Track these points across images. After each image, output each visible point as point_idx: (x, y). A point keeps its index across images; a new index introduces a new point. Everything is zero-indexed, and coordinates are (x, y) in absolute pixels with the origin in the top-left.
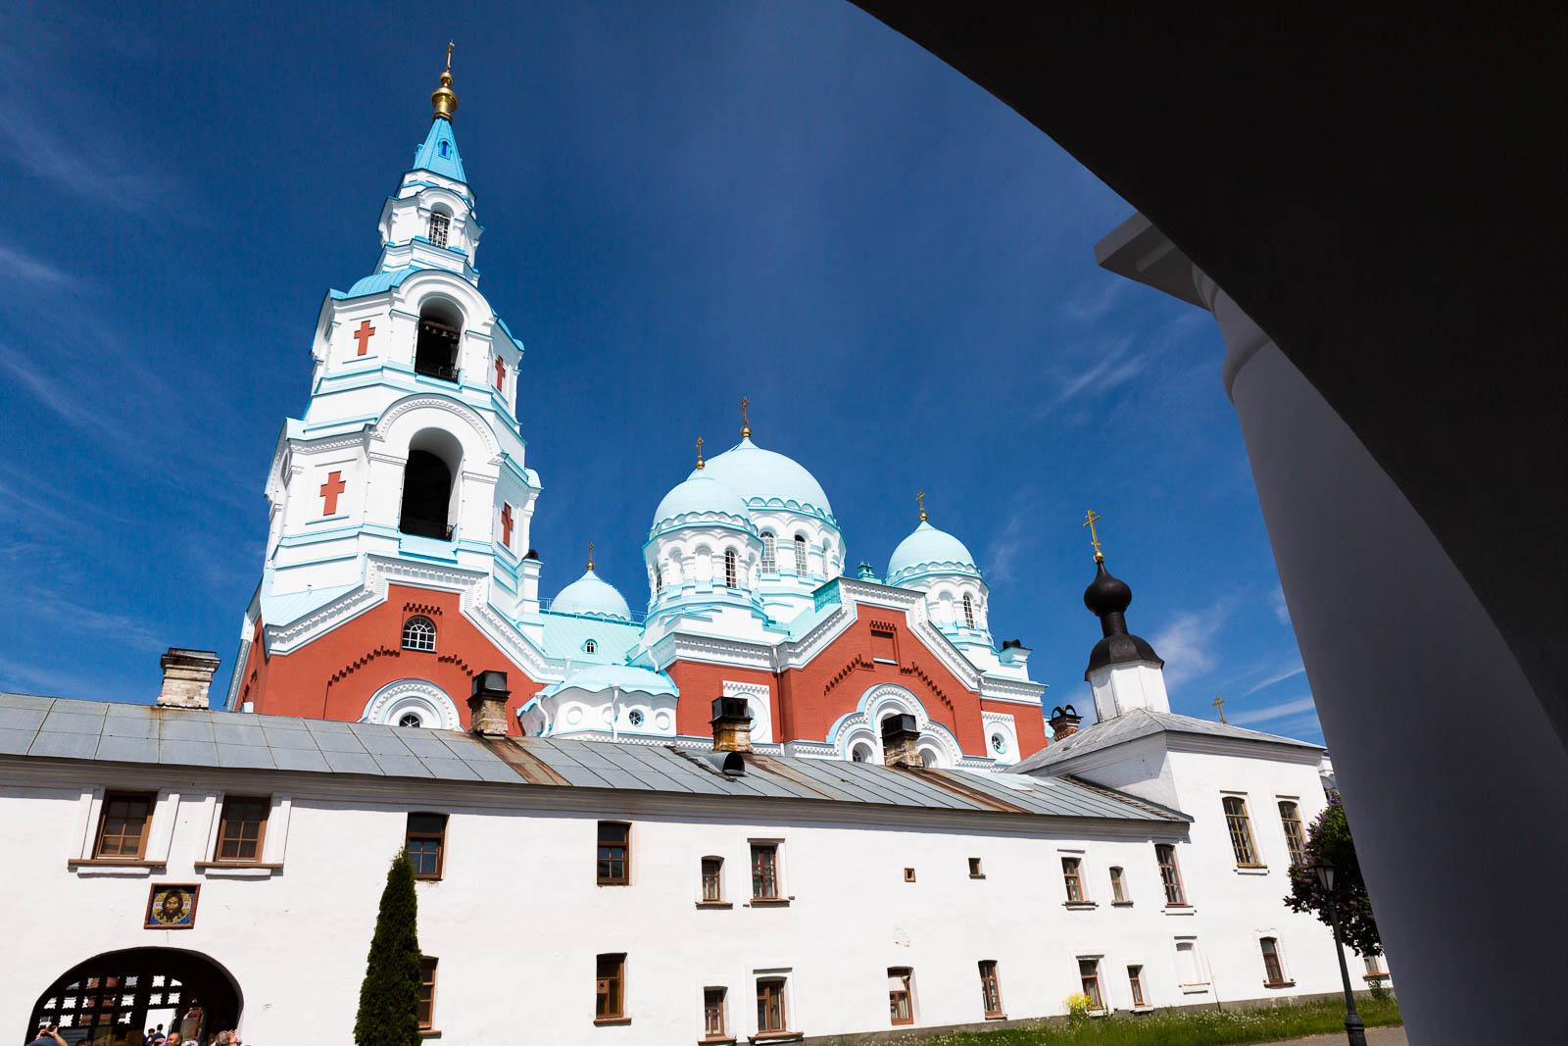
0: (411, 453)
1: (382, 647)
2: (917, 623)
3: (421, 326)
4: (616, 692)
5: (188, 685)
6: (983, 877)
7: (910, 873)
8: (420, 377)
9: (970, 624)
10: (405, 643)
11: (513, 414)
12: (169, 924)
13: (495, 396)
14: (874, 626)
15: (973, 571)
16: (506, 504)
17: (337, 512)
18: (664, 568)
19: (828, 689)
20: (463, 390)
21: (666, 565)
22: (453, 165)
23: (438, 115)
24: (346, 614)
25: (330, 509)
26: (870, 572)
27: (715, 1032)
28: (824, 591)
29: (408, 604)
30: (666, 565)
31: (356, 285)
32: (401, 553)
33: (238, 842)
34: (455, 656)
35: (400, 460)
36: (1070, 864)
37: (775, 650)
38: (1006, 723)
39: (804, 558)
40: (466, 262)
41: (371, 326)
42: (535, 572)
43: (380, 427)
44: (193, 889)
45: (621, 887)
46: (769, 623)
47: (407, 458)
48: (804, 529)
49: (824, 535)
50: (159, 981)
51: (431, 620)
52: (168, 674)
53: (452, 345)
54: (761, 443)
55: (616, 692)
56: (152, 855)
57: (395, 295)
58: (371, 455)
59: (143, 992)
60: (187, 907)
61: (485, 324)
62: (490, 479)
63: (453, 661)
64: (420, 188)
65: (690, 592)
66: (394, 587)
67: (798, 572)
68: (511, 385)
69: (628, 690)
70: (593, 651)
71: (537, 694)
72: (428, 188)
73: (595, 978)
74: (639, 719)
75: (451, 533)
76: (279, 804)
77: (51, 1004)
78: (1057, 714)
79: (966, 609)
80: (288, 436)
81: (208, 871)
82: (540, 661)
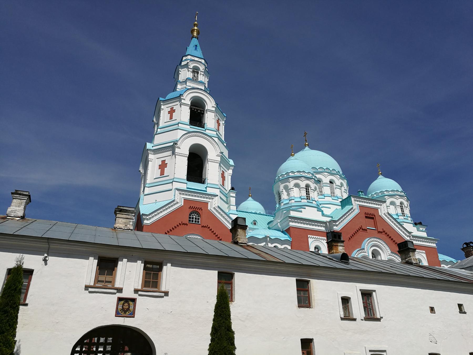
3: (191, 109)
4: (268, 238)
5: (124, 221)
6: (465, 313)
7: (432, 309)
9: (403, 214)
10: (190, 221)
11: (223, 140)
12: (125, 315)
13: (217, 132)
14: (366, 214)
15: (403, 194)
17: (165, 174)
19: (350, 239)
20: (207, 130)
22: (199, 53)
23: (193, 37)
24: (169, 210)
25: (162, 173)
26: (363, 194)
28: (344, 203)
29: (190, 207)
31: (169, 95)
32: (187, 188)
33: (151, 281)
34: (207, 225)
35: (186, 155)
38: (422, 254)
39: (333, 190)
40: (205, 86)
42: (234, 195)
43: (179, 143)
44: (134, 300)
45: (306, 309)
48: (334, 179)
49: (341, 181)
51: (197, 211)
52: (118, 215)
53: (201, 115)
54: (312, 148)
55: (268, 238)
56: (117, 285)
57: (182, 97)
60: (131, 308)
61: (213, 107)
62: (217, 162)
63: (206, 227)
65: (293, 201)
66: (185, 200)
67: (332, 195)
68: (222, 129)
69: (272, 238)
70: (256, 224)
72: (191, 61)
73: (301, 349)
75: (205, 179)
76: (166, 265)
77: (78, 349)
78: (465, 246)
79: (401, 208)
80: (147, 148)
81: (140, 293)
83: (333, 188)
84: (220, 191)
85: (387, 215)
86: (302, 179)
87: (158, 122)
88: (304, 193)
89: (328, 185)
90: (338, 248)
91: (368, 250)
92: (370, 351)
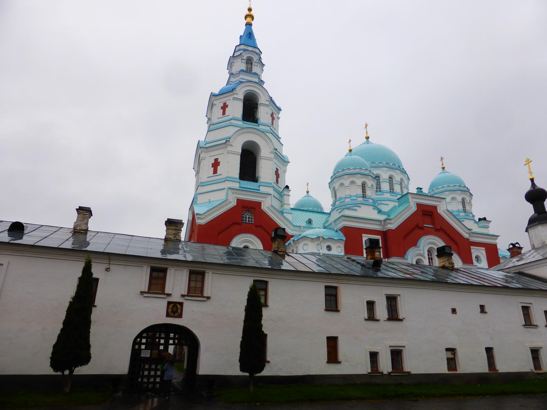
0: (242, 150)
1: (235, 222)
2: (442, 210)
4: (321, 239)
5: (174, 232)
7: (454, 311)
8: (245, 122)
13: (271, 127)
16: (276, 168)
18: (338, 191)
21: (338, 189)
27: (374, 369)
29: (243, 206)
30: (338, 189)
34: (261, 225)
36: (526, 310)
37: (383, 222)
39: (393, 186)
41: (227, 104)
43: (231, 140)
44: (181, 304)
46: (380, 212)
47: (241, 152)
50: (172, 335)
53: (255, 109)
55: (321, 239)
58: (228, 152)
59: (167, 339)
61: (267, 100)
64: (241, 51)
67: (390, 191)
70: (311, 223)
71: (291, 239)
72: (244, 51)
74: (330, 249)
78: (511, 246)
81: (186, 298)
82: (291, 227)
83: (393, 184)
84: (273, 189)
85: (446, 212)
86: (358, 176)
87: (211, 118)
88: (360, 192)
89: (386, 181)
90: (374, 254)
91: (424, 248)
92: (390, 346)
